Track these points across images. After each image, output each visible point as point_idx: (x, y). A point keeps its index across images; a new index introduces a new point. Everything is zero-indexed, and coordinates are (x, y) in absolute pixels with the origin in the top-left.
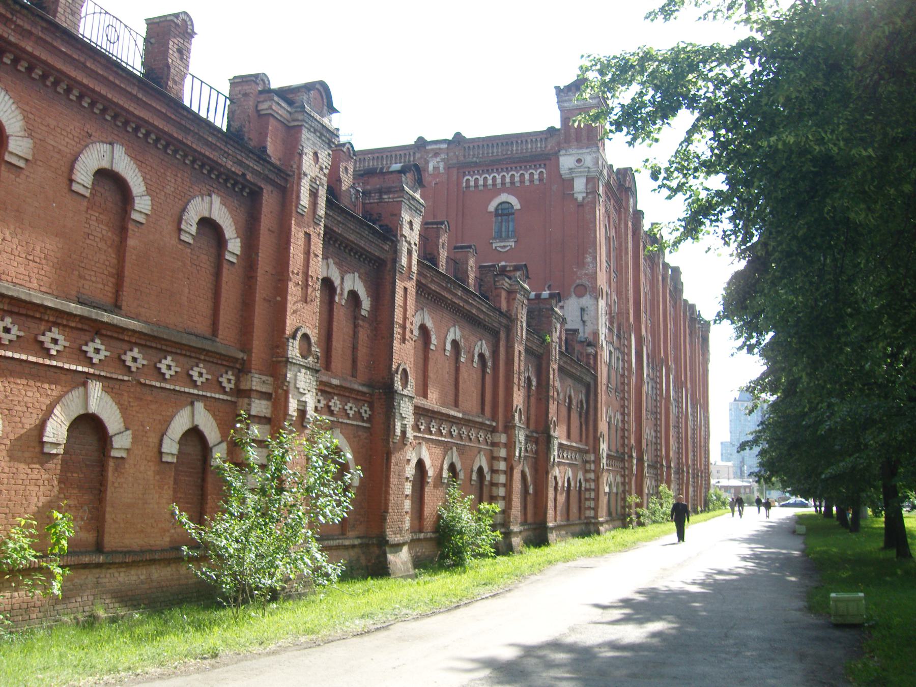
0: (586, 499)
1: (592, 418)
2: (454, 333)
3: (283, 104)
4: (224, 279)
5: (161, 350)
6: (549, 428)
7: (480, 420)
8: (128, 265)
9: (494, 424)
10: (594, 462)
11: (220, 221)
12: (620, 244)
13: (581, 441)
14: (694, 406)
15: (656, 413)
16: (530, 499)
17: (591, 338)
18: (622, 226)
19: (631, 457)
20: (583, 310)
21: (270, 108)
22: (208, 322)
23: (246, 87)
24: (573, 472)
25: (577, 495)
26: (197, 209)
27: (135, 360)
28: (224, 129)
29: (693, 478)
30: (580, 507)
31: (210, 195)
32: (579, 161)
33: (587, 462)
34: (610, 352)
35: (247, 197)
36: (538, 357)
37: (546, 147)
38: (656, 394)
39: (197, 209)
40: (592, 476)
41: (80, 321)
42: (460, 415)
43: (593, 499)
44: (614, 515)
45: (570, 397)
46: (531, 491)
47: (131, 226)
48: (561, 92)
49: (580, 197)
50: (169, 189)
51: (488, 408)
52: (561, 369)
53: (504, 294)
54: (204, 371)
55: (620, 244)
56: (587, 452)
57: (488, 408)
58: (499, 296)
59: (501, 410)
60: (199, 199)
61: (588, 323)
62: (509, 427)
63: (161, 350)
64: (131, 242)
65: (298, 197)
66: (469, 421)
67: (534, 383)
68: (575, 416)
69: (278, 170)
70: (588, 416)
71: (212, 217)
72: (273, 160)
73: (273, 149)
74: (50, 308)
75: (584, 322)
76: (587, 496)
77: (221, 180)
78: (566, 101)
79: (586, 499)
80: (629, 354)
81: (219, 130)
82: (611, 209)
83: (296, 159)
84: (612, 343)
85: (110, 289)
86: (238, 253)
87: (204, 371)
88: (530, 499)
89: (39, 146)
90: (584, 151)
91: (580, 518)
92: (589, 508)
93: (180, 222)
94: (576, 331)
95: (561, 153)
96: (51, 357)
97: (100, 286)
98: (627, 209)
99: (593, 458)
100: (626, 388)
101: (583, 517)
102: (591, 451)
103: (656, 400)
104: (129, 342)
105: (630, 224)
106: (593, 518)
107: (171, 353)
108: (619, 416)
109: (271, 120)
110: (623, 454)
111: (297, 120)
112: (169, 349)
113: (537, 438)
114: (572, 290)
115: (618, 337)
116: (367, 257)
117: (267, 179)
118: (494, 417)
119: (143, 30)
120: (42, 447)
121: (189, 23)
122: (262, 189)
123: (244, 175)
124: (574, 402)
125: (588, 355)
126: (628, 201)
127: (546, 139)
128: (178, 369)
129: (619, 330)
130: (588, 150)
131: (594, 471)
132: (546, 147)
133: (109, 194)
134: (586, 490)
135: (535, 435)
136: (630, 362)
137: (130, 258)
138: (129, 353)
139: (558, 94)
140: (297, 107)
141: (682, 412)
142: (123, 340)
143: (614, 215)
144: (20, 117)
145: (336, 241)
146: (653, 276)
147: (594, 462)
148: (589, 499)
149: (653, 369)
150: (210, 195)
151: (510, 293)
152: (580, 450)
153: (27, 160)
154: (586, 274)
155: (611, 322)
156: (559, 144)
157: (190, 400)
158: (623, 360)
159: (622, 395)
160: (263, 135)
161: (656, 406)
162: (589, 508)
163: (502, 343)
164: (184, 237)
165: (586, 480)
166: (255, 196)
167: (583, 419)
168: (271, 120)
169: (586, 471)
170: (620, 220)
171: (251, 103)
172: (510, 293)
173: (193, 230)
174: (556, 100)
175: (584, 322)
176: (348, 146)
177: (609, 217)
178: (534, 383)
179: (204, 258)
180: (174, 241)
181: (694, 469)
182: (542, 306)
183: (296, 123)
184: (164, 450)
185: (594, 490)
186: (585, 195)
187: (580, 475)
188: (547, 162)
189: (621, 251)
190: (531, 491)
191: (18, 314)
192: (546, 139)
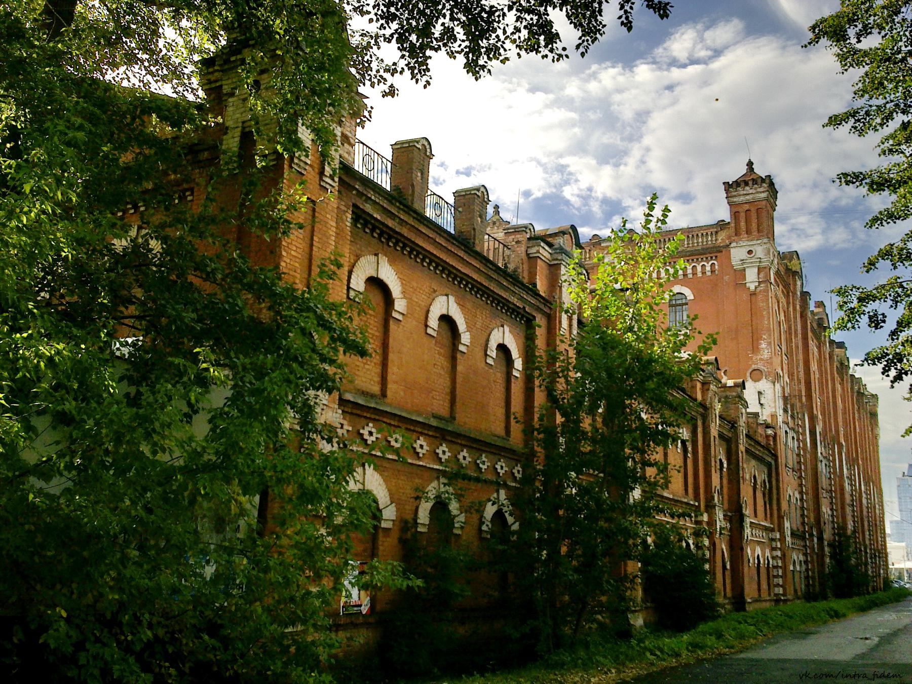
0: (774, 577)
1: (775, 497)
2: (445, 304)
3: (547, 248)
4: (513, 391)
5: (479, 449)
6: (741, 507)
7: (686, 500)
8: (458, 386)
9: (697, 504)
10: (780, 540)
11: (391, 286)
12: (790, 328)
13: (766, 520)
14: (867, 484)
15: (831, 490)
16: (728, 573)
17: (769, 421)
18: (791, 309)
19: (811, 535)
20: (760, 393)
21: (538, 252)
22: (503, 425)
23: (518, 236)
24: (762, 551)
25: (765, 571)
26: (496, 338)
27: (464, 458)
28: (389, 189)
29: (871, 558)
30: (769, 585)
31: (503, 326)
32: (750, 252)
33: (773, 540)
34: (786, 432)
35: (526, 323)
36: (729, 442)
37: (716, 240)
38: (830, 472)
39: (496, 338)
40: (779, 553)
41: (435, 431)
42: (671, 497)
43: (781, 577)
44: (799, 593)
45: (755, 477)
46: (728, 567)
47: (459, 356)
48: (728, 186)
49: (752, 287)
50: (479, 325)
51: (690, 491)
52: (747, 451)
53: (699, 385)
54: (374, 430)
55: (790, 328)
56: (772, 530)
57: (690, 491)
58: (694, 387)
59: (702, 491)
60: (496, 330)
61: (766, 406)
62: (710, 507)
63: (479, 449)
64: (460, 368)
65: (560, 322)
66: (678, 501)
67: (725, 465)
68: (759, 495)
69: (546, 301)
70: (771, 493)
71: (450, 314)
72: (543, 295)
73: (541, 286)
74: (349, 401)
75: (762, 405)
76: (775, 574)
77: (391, 244)
78: (735, 196)
79: (774, 577)
80: (804, 434)
81: (384, 190)
82: (780, 294)
83: (558, 291)
84: (787, 424)
85: (447, 404)
86: (521, 369)
87: (374, 430)
88: (728, 573)
89: (410, 305)
90: (755, 242)
91: (769, 594)
92: (778, 585)
93: (486, 351)
94: (756, 415)
95: (732, 245)
96: (419, 458)
97: (441, 403)
98: (794, 293)
99: (778, 537)
100: (803, 467)
101: (772, 594)
102: (776, 529)
103: (830, 478)
104: (461, 444)
105: (798, 307)
106: (782, 595)
107: (485, 451)
108: (797, 495)
109: (539, 261)
110: (804, 532)
111: (557, 259)
112: (483, 448)
113: (731, 517)
114: (748, 374)
115: (792, 417)
116: (468, 283)
117: (538, 309)
118: (697, 497)
119: (388, 154)
120: (417, 527)
121: (428, 147)
122: (534, 317)
123: (524, 308)
124: (759, 482)
125: (767, 436)
126: (795, 285)
127: (716, 232)
128: (379, 436)
129: (792, 410)
130: (759, 242)
131: (780, 549)
132: (716, 240)
133: (376, 298)
134: (774, 567)
135: (729, 514)
136: (804, 441)
137: (459, 379)
138: (418, 442)
139: (727, 191)
140: (556, 249)
141: (856, 490)
142: (457, 443)
143: (783, 300)
144: (400, 284)
145: (418, 253)
146: (820, 356)
147: (780, 540)
148: (777, 576)
149: (825, 447)
150: (503, 326)
151: (705, 384)
152: (766, 529)
153: (403, 314)
154: (761, 359)
155: (785, 404)
156: (729, 237)
157: (436, 475)
158: (798, 440)
159: (798, 474)
160: (533, 274)
161: (830, 485)
162: (778, 585)
163: (700, 430)
164: (429, 331)
165: (773, 558)
166: (529, 323)
167: (767, 499)
168: (539, 261)
169: (773, 549)
170: (788, 303)
171: (523, 249)
172: (705, 384)
173: (494, 354)
174: (725, 195)
175: (762, 405)
176: (482, 189)
177: (778, 302)
178: (725, 465)
179: (499, 375)
180: (483, 364)
181: (871, 549)
182: (728, 393)
183: (556, 262)
184: (419, 521)
185: (781, 567)
186: (757, 284)
187: (768, 553)
188: (718, 254)
189: (790, 334)
190: (728, 567)
191: (472, 448)
192: (716, 232)
